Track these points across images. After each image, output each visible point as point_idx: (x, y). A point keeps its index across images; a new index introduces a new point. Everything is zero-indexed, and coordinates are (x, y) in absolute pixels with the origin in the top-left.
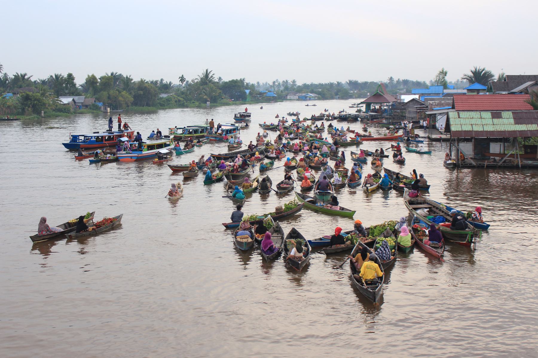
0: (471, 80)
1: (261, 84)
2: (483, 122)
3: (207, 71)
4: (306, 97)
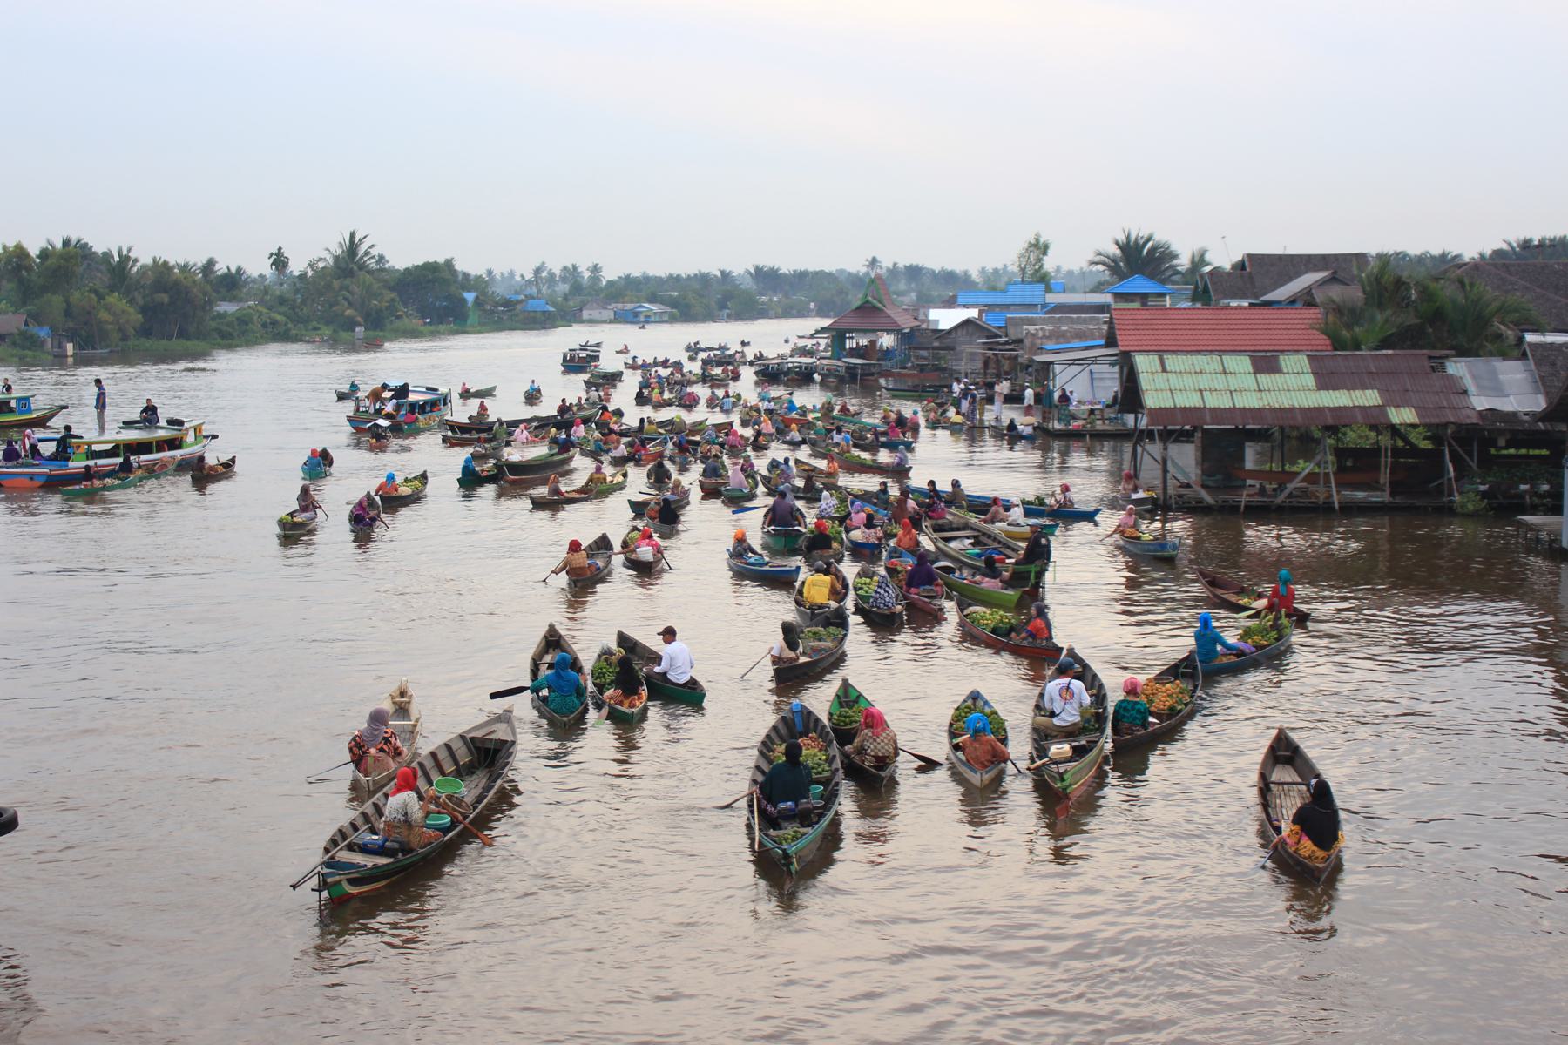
0: (1113, 266)
2: (1231, 383)
3: (352, 235)
4: (636, 314)
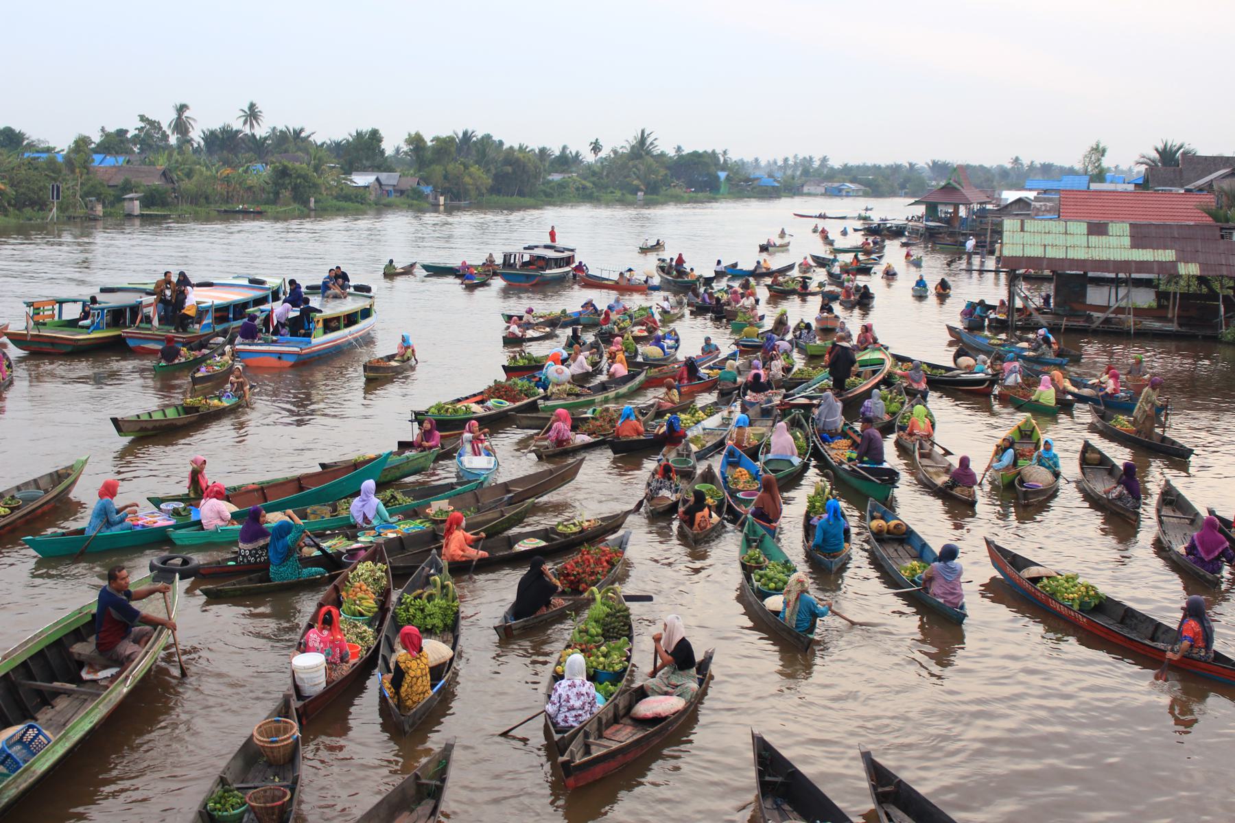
1: (763, 163)
3: (643, 132)
4: (840, 190)
